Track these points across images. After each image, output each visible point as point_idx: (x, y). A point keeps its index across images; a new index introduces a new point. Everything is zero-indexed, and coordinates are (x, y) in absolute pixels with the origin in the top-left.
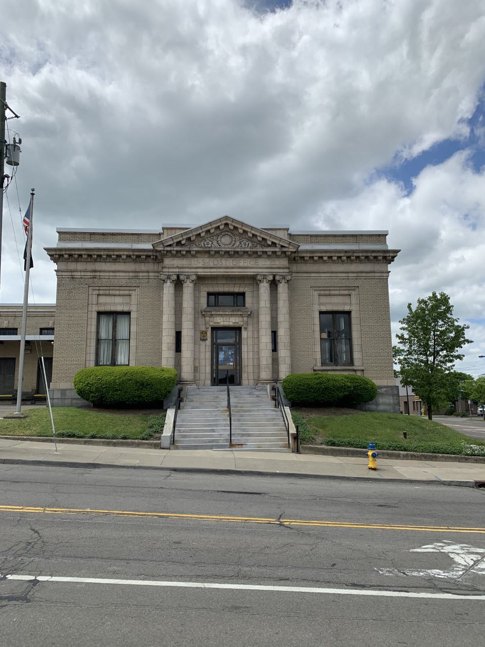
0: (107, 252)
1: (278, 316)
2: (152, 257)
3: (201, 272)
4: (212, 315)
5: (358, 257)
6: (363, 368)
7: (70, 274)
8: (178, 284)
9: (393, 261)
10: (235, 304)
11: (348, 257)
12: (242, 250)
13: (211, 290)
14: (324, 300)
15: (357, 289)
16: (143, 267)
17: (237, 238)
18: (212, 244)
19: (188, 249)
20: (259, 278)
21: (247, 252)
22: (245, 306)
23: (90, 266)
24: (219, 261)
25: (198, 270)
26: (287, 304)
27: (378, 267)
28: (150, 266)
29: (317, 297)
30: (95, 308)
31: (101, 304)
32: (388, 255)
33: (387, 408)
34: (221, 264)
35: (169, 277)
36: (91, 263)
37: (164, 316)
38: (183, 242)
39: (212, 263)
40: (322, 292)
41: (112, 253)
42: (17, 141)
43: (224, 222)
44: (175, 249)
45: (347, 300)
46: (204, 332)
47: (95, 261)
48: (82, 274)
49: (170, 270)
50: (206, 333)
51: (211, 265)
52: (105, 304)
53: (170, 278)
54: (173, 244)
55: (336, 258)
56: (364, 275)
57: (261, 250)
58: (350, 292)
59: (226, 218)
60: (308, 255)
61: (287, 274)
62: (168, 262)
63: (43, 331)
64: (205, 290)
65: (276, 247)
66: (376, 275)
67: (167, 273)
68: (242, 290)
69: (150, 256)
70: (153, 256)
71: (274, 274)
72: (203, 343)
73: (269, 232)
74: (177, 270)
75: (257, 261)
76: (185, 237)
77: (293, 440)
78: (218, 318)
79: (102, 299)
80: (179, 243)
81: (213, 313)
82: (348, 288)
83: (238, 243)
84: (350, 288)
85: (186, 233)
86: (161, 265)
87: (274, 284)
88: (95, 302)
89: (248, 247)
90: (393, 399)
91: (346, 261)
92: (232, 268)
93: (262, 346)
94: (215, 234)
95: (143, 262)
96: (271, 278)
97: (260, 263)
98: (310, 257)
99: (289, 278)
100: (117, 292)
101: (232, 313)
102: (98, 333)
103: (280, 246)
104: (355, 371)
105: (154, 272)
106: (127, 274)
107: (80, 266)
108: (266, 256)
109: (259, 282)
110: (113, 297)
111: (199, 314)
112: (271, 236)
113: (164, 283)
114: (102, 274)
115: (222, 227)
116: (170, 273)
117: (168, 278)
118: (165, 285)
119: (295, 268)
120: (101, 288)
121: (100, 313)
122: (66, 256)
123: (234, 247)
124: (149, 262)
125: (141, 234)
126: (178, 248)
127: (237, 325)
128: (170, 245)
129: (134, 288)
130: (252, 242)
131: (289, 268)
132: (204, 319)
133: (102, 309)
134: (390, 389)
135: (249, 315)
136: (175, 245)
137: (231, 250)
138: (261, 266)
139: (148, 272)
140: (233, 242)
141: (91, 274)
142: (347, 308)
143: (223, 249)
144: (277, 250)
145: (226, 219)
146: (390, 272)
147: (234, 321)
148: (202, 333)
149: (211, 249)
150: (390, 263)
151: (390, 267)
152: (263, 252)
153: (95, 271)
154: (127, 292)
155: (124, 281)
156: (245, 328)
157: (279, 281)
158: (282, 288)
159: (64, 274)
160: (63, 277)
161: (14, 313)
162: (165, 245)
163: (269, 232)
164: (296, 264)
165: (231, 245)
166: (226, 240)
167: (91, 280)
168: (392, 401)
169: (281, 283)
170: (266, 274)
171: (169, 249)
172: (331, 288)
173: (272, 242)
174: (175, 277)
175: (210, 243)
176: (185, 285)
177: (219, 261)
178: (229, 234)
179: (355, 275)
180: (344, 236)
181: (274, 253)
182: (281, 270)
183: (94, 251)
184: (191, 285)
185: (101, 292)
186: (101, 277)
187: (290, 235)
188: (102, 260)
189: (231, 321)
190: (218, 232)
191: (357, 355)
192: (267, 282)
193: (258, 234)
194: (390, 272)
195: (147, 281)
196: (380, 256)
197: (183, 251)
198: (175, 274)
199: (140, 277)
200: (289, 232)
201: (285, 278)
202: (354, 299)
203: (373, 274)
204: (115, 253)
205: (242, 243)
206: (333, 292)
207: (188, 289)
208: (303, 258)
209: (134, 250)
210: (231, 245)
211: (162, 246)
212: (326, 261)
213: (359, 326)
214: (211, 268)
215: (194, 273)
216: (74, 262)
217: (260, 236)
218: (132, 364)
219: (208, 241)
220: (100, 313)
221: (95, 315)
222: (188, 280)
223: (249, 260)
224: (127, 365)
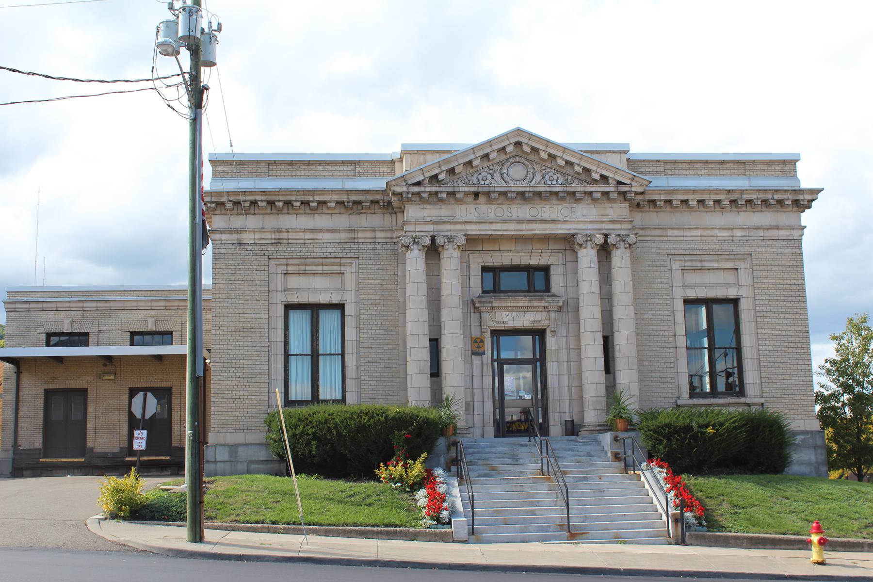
0: (303, 197)
1: (614, 309)
2: (381, 204)
3: (474, 230)
4: (493, 307)
5: (749, 201)
6: (762, 401)
7: (234, 236)
8: (433, 251)
9: (809, 207)
10: (531, 290)
11: (733, 202)
12: (548, 189)
13: (489, 261)
14: (691, 278)
15: (749, 258)
16: (364, 221)
17: (537, 168)
18: (492, 178)
19: (450, 190)
20: (579, 239)
21: (557, 193)
22: (549, 292)
23: (271, 222)
24: (505, 209)
25: (468, 227)
26: (629, 287)
27: (783, 218)
28: (376, 220)
29: (677, 274)
30: (281, 299)
31: (290, 290)
32: (801, 197)
33: (805, 469)
34: (510, 215)
35: (416, 241)
36: (271, 215)
37: (408, 313)
38: (441, 177)
39: (492, 214)
40: (688, 265)
41: (310, 198)
42: (215, 27)
43: (513, 140)
44: (428, 189)
45: (730, 277)
46: (478, 340)
47: (280, 211)
48: (257, 236)
49: (419, 228)
50: (482, 341)
51: (492, 217)
52: (298, 290)
53: (418, 242)
54: (423, 180)
55: (711, 203)
56: (761, 232)
57: (582, 189)
58: (737, 263)
59: (519, 131)
60: (663, 197)
61: (628, 233)
62: (413, 212)
63: (136, 337)
64: (478, 261)
65: (608, 184)
66: (781, 232)
67: (414, 234)
68: (543, 262)
69: (377, 202)
70: (384, 201)
71: (606, 232)
72: (476, 359)
73: (594, 156)
74: (430, 227)
75: (573, 210)
76: (444, 168)
77: (674, 523)
78: (503, 314)
79: (294, 282)
80: (434, 179)
81: (494, 305)
82: (732, 257)
83: (538, 178)
84: (737, 257)
85: (447, 161)
86: (400, 218)
87: (605, 250)
88: (280, 287)
89: (554, 182)
90: (816, 454)
91: (729, 209)
92: (530, 222)
93: (587, 364)
94: (497, 160)
95: (365, 213)
96: (600, 240)
97: (579, 213)
98: (666, 201)
99: (632, 239)
100: (319, 269)
101: (529, 304)
102: (286, 343)
103: (616, 183)
104: (749, 405)
105: (385, 231)
106: (337, 235)
107: (253, 221)
108: (589, 201)
109: (577, 247)
110: (312, 278)
111: (473, 306)
112: (599, 163)
113: (407, 251)
114: (291, 236)
115: (510, 149)
116: (418, 234)
117: (414, 242)
118: (409, 255)
119: (639, 218)
120: (290, 261)
121: (288, 307)
122: (229, 205)
123: (533, 182)
124: (375, 213)
125: (359, 161)
126: (434, 189)
127: (538, 326)
128: (418, 184)
129: (348, 261)
130: (563, 174)
131: (631, 221)
132: (477, 315)
133: (294, 299)
134: (809, 436)
135: (561, 307)
136: (427, 181)
137: (527, 189)
138: (582, 218)
139: (374, 230)
140: (531, 175)
141: (273, 236)
142: (732, 293)
143: (514, 189)
144: (611, 189)
145: (518, 135)
146: (805, 227)
147: (533, 319)
148: (476, 342)
149: (492, 189)
150: (803, 211)
151: (806, 217)
152: (586, 193)
153: (279, 231)
154: (336, 269)
155: (331, 247)
156: (552, 331)
157: (614, 245)
158: (620, 258)
159: (224, 236)
160: (223, 242)
161: (80, 305)
162: (410, 182)
163: (594, 156)
164: (640, 214)
165: (526, 181)
166: (516, 172)
167: (272, 248)
168: (813, 458)
169: (617, 248)
170: (591, 232)
171: (416, 189)
172: (703, 257)
173: (602, 176)
174: (427, 241)
175: (489, 177)
176: (444, 254)
177: (505, 209)
178: (523, 160)
179: (745, 233)
180: (723, 162)
181: (606, 194)
182: (618, 226)
183: (278, 195)
184: (456, 254)
185: (291, 269)
186: (290, 241)
187: (628, 160)
188: (274, 211)
189: (528, 319)
190: (503, 157)
191: (751, 378)
192: (592, 248)
193: (576, 161)
194: (805, 227)
195: (371, 246)
196: (787, 200)
197: (441, 192)
198: (427, 236)
199: (360, 241)
200: (628, 156)
201: (624, 241)
202: (744, 277)
203: (775, 232)
204: (317, 198)
205: (547, 177)
206: (706, 265)
207: (451, 260)
208: (653, 202)
209: (349, 192)
210: (526, 181)
211: (404, 184)
212: (693, 207)
213: (753, 325)
214: (491, 222)
215: (462, 233)
216: (242, 214)
217: (578, 165)
218: (352, 398)
219: (484, 174)
220: (288, 307)
221: (281, 311)
222: (450, 245)
223: (560, 207)
224: (338, 401)
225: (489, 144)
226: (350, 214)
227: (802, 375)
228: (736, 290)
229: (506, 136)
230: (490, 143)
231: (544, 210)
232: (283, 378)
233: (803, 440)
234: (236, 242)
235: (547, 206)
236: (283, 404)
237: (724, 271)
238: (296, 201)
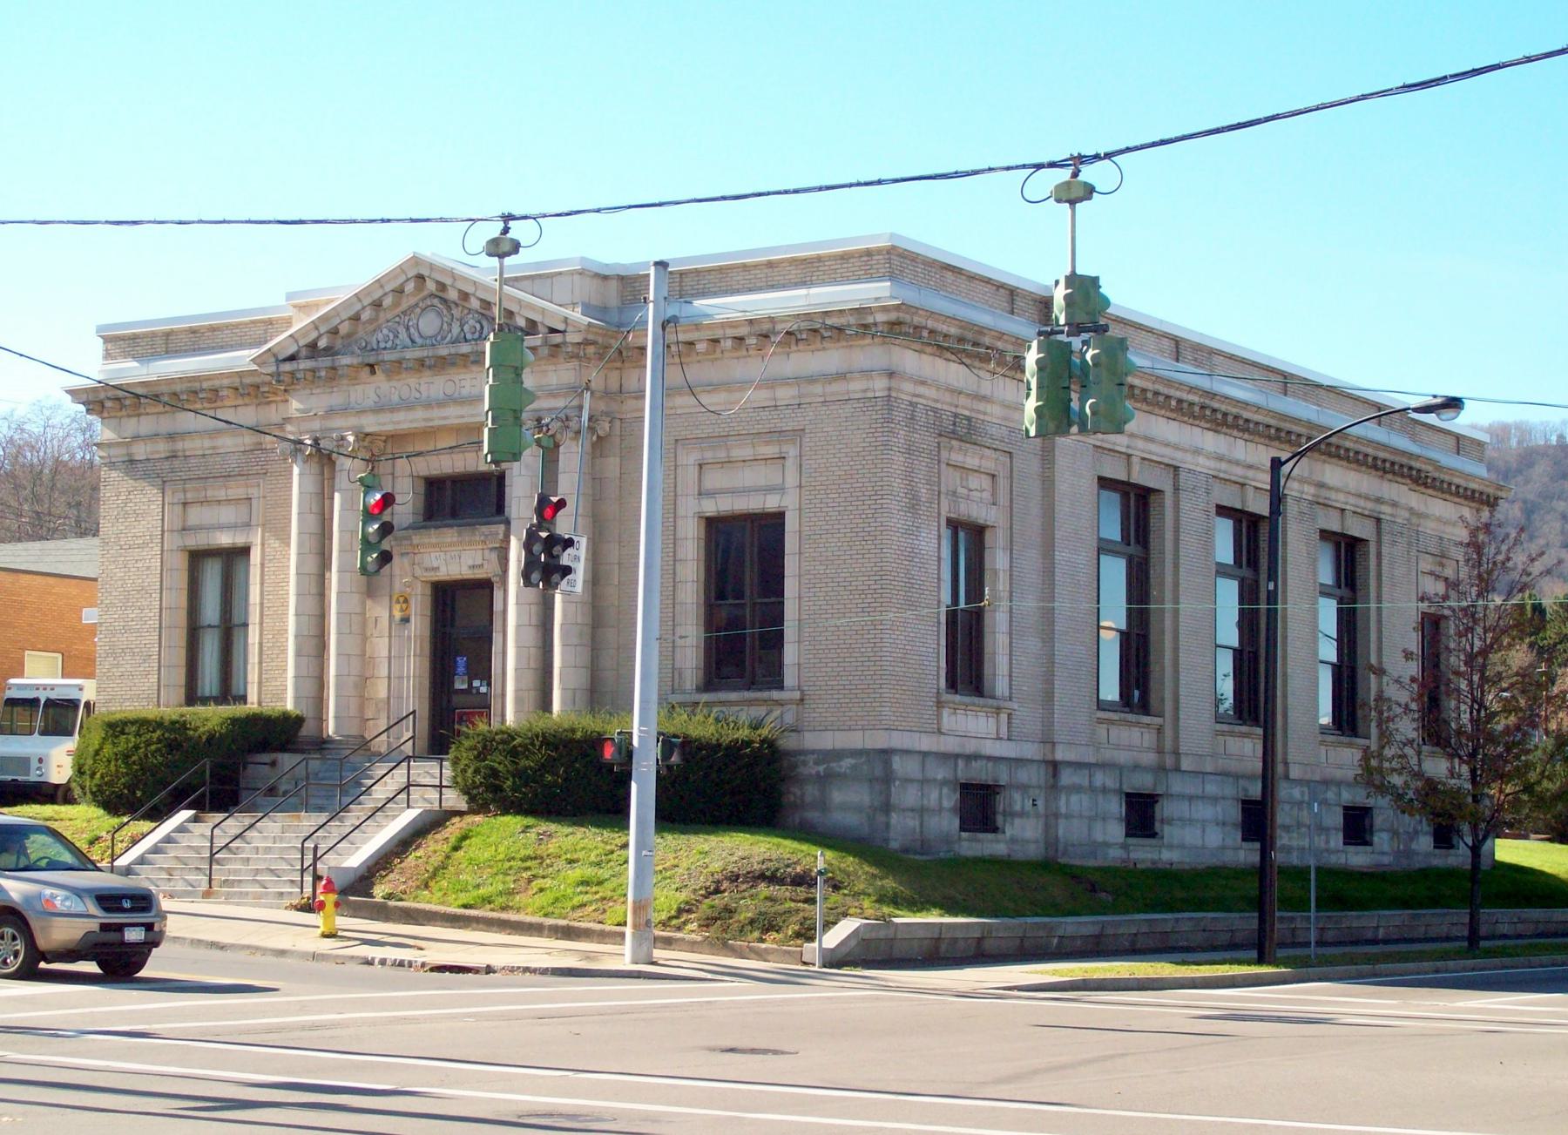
23: (166, 423)
54: (298, 352)
55: (729, 343)
59: (415, 260)
85: (323, 318)
162: (281, 358)
167: (166, 464)
206: (737, 453)
225: (377, 285)
226: (258, 405)
227: (869, 650)
228: (778, 497)
229: (401, 269)
230: (379, 283)
231: (463, 383)
232: (183, 662)
233: (854, 767)
234: (126, 458)
235: (468, 376)
236: (691, 657)
237: (769, 462)
238: (182, 392)
